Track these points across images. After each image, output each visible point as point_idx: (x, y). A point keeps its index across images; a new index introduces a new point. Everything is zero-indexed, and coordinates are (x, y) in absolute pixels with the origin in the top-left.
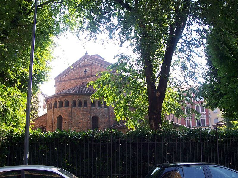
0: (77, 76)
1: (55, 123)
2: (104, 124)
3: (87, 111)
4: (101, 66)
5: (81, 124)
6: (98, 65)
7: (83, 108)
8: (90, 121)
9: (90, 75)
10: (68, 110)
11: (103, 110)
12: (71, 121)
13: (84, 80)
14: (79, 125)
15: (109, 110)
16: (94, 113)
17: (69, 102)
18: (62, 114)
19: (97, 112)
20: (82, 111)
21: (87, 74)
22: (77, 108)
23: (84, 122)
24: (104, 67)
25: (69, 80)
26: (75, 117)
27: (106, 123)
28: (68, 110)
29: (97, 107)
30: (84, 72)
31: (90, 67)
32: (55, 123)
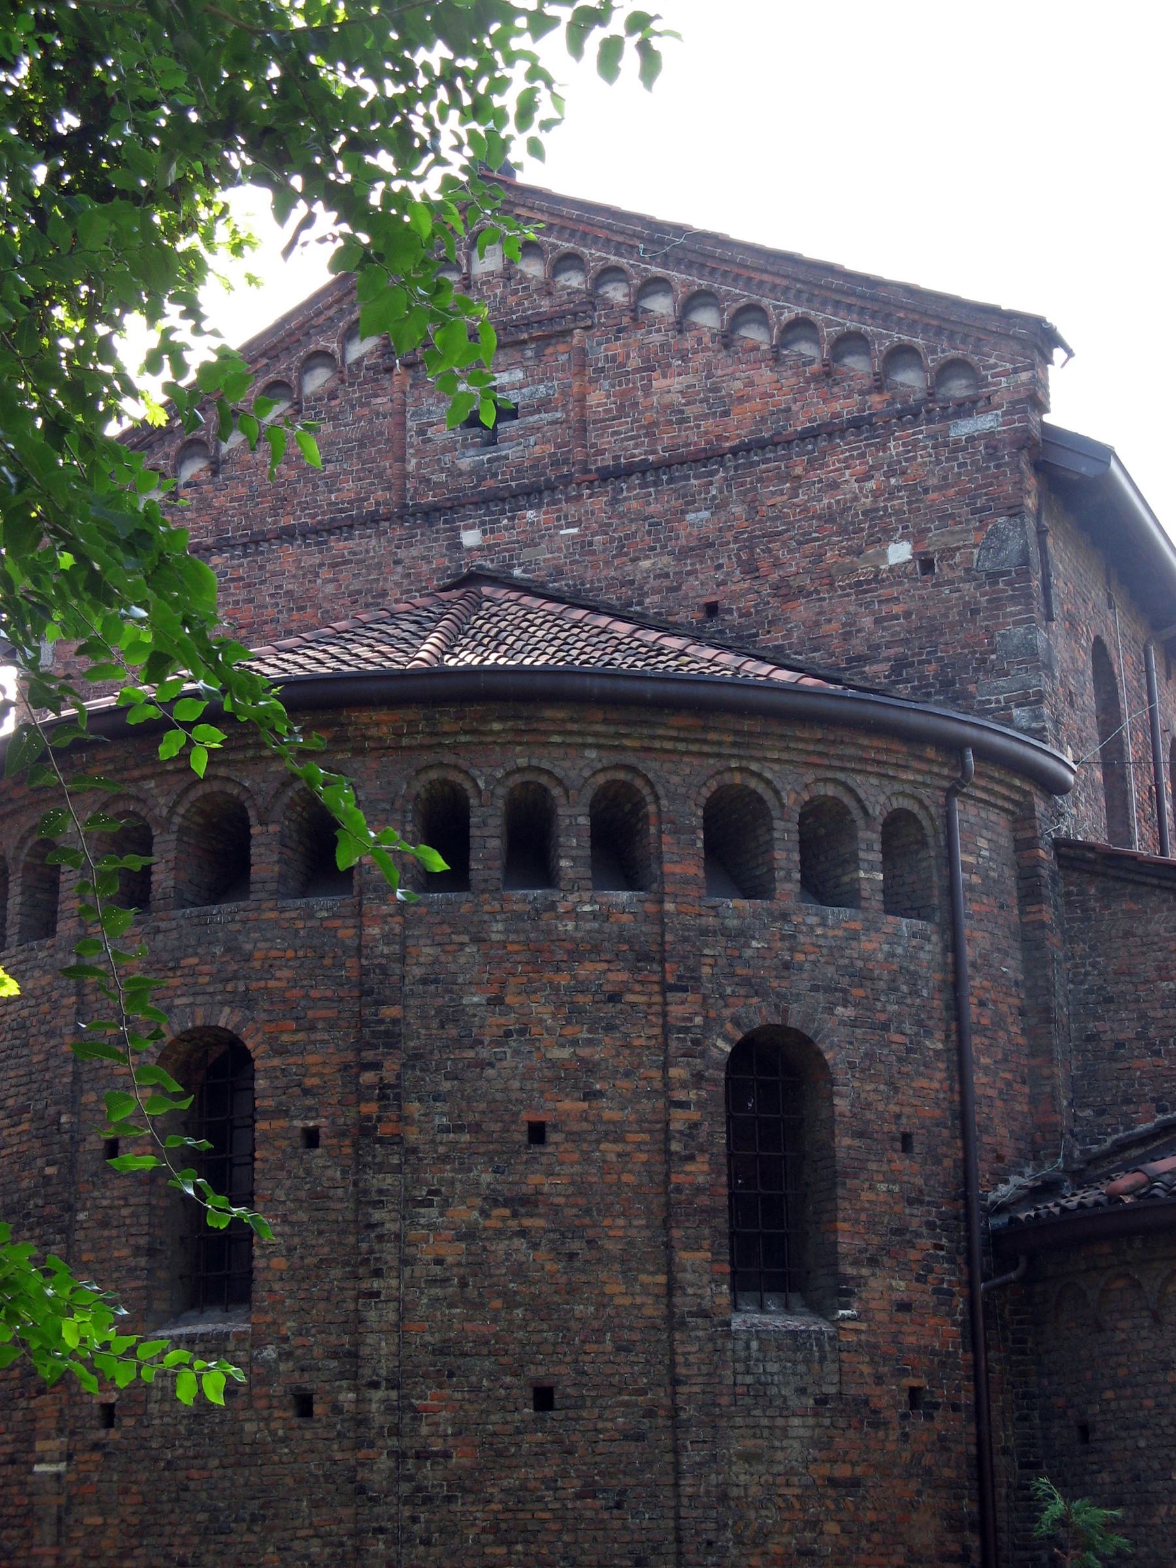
0: (350, 487)
2: (901, 1163)
3: (646, 956)
4: (727, 339)
6: (681, 325)
7: (582, 904)
8: (700, 1111)
10: (347, 934)
11: (872, 944)
13: (471, 538)
14: (535, 1179)
15: (954, 946)
16: (754, 987)
18: (247, 1001)
19: (787, 966)
20: (576, 955)
21: (519, 449)
22: (501, 909)
23: (616, 1133)
24: (783, 344)
25: (222, 545)
26: (458, 1043)
28: (347, 934)
29: (788, 887)
31: (560, 354)
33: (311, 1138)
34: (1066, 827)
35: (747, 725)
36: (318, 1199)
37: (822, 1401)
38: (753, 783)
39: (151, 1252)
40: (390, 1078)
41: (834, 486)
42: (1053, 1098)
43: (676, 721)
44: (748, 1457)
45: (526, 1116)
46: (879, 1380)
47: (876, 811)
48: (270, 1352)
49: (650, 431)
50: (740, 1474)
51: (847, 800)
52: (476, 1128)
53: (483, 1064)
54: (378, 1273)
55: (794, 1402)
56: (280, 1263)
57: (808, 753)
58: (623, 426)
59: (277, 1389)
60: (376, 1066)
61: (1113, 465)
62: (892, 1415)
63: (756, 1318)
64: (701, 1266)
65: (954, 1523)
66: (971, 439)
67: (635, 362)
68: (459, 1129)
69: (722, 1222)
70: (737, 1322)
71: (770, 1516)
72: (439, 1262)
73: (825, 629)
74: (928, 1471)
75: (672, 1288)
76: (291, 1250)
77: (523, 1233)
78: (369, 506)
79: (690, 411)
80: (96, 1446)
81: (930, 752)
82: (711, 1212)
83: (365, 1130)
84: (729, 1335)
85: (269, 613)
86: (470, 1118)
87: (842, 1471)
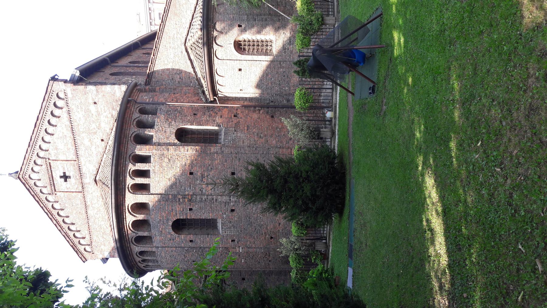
1: (191, 241)
2: (199, 115)
5: (195, 168)
9: (74, 166)
12: (188, 195)
14: (199, 174)
17: (136, 204)
18: (168, 220)
27: (196, 113)
30: (66, 181)
32: (191, 241)
33: (191, 209)
34: (142, 83)
36: (201, 208)
38: (133, 136)
39: (208, 235)
40: (181, 197)
41: (80, 118)
42: (188, 90)
43: (122, 138)
45: (188, 175)
46: (232, 121)
48: (225, 216)
49: (68, 149)
50: (246, 144)
51: (136, 120)
52: (190, 183)
54: (213, 199)
56: (210, 215)
58: (67, 154)
59: (230, 215)
60: (179, 199)
61: (360, 50)
62: (238, 120)
63: (222, 140)
64: (214, 149)
65: (254, 111)
66: (72, 94)
67: (56, 151)
68: (190, 186)
69: (207, 145)
70: (223, 143)
72: (211, 189)
73: (106, 121)
75: (217, 153)
76: (209, 213)
77: (207, 176)
78: (81, 198)
79: (65, 142)
80: (238, 243)
81: (129, 105)
82: (205, 146)
83: (190, 200)
84: (224, 145)
85: (101, 215)
86: (188, 184)
87: (246, 128)
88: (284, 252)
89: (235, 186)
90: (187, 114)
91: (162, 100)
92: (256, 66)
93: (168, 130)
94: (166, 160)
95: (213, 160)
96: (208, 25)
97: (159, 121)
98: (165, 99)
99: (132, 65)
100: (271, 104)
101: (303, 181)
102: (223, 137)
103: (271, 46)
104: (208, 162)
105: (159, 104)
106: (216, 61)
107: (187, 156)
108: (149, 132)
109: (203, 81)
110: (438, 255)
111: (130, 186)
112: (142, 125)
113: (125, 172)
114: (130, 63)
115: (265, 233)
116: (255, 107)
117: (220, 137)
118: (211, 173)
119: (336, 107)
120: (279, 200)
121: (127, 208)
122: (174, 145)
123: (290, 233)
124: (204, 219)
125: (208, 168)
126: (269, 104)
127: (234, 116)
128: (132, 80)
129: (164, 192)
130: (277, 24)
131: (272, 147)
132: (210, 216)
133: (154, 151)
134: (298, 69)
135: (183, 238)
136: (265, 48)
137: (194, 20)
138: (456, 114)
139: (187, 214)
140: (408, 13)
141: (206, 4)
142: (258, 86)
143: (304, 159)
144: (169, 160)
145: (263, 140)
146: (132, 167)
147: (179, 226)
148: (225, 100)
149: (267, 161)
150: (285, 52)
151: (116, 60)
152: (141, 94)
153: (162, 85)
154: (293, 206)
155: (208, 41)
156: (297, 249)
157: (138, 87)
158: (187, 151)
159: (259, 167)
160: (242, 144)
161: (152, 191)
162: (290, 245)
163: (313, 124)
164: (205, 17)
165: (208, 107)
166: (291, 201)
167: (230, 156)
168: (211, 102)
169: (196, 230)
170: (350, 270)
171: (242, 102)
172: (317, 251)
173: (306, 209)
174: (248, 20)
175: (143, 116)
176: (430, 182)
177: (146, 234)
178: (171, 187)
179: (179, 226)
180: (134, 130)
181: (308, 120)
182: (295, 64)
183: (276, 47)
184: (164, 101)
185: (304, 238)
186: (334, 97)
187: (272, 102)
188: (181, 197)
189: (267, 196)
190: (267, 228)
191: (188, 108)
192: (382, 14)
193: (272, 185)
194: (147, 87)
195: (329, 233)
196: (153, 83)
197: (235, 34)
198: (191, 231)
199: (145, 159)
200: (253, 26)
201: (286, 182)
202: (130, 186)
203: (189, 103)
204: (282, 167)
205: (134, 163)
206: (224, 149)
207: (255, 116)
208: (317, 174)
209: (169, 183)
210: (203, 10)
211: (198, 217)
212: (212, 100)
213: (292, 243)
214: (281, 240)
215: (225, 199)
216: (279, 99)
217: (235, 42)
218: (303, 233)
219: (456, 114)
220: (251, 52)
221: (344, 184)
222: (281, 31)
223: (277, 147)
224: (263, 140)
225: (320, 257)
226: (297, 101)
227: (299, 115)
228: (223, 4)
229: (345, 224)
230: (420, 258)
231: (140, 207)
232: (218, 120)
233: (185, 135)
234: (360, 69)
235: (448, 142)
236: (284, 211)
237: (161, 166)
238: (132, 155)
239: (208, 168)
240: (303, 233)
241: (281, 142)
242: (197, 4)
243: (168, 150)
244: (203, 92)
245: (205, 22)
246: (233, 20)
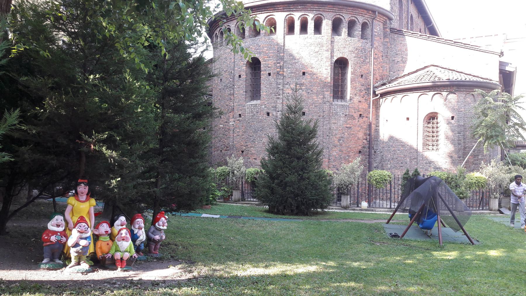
1: (240, 76)
2: (361, 79)
5: (309, 77)
14: (303, 81)
17: (275, 21)
18: (260, 53)
27: (364, 77)
32: (240, 76)
34: (392, 26)
35: (340, 7)
36: (271, 84)
37: (346, 115)
38: (341, 17)
39: (246, 92)
40: (281, 65)
44: (334, 123)
47: (361, 22)
48: (263, 107)
50: (333, 126)
51: (356, 20)
52: (295, 73)
53: (296, 63)
54: (279, 95)
55: (342, 115)
57: (449, 255)
60: (279, 63)
64: (328, 94)
65: (365, 134)
68: (292, 73)
70: (333, 103)
71: (337, 132)
74: (362, 126)
75: (324, 98)
81: (370, 12)
82: (330, 86)
83: (278, 73)
87: (348, 126)
88: (231, 161)
89: (295, 110)
90: (362, 69)
91: (376, 44)
92: (411, 135)
93: (346, 50)
94: (317, 50)
95: (317, 94)
96: (454, 86)
97: (356, 42)
98: (377, 47)
99: (410, 17)
100: (373, 151)
101: (299, 175)
102: (340, 103)
103: (433, 149)
104: (315, 89)
105: (372, 41)
106: (416, 95)
107: (321, 70)
108: (344, 31)
109: (395, 83)
110: (245, 270)
111: (292, 16)
112: (351, 25)
113: (305, 9)
114: (412, 16)
115: (247, 145)
116: (369, 135)
117: (339, 100)
118: (304, 92)
119: (372, 211)
120: (281, 152)
121: (271, 14)
122: (332, 57)
123: (247, 167)
124: (260, 88)
125: (309, 89)
126: (371, 149)
127: (360, 115)
128: (395, 16)
129: (286, 48)
130: (455, 156)
131: (329, 152)
132: (263, 93)
133: (326, 37)
134: (411, 174)
135: (242, 68)
136: (430, 143)
137: (457, 73)
138: (383, 288)
139: (265, 70)
140: (479, 262)
141: (475, 83)
142: (391, 138)
143: (321, 176)
144: (317, 52)
145: (336, 142)
146: (310, 17)
147: (255, 65)
148: (377, 106)
149: (317, 141)
150: (426, 163)
151: (414, 2)
152: (381, 25)
153: (391, 44)
154: (275, 166)
155: (436, 87)
156: (233, 173)
157: (388, 22)
158: (326, 69)
159: (312, 133)
160: (332, 122)
161: (288, 37)
162: (238, 166)
163: (354, 189)
164: (462, 83)
165: (369, 89)
166: (281, 163)
167: (321, 110)
168: (374, 92)
169: (250, 80)
170: (218, 216)
171: (374, 122)
172: (232, 192)
173: (272, 178)
174: (459, 126)
175: (360, 26)
176: (312, 268)
177: (247, 33)
178: (291, 55)
179: (255, 65)
180: (346, 18)
181: (358, 184)
182: (416, 171)
183: (431, 155)
184: (375, 46)
185: (244, 180)
186: (382, 209)
187: (375, 152)
188: (281, 65)
189: (285, 140)
190: (251, 147)
191: (368, 70)
192: (473, 244)
193: (294, 146)
194: (388, 30)
195: (248, 204)
196: (393, 35)
197: (444, 114)
198: (250, 76)
199: (318, 28)
200: (453, 131)
201: (299, 158)
202: (292, 16)
203: (374, 70)
204: (312, 156)
205: (314, 18)
206: (328, 104)
207: (361, 135)
208: (306, 188)
209: (294, 53)
210: (468, 82)
211: (262, 82)
212: (377, 93)
213: (239, 168)
214: (241, 158)
215: (280, 107)
216: (378, 159)
217: (437, 113)
218: (248, 178)
219: (383, 288)
220: (426, 129)
221: (297, 214)
222: (449, 160)
223: (329, 156)
224: (336, 142)
225: (227, 194)
226: (376, 173)
227: (363, 175)
228: (475, 101)
229: (259, 214)
230: (239, 258)
231: (272, 24)
232: (356, 99)
233: (341, 68)
234: (415, 224)
235: (355, 281)
236: (269, 157)
237: (311, 45)
238: (322, 17)
239: (309, 89)
240: (248, 178)
241: (335, 161)
242: (474, 76)
243: (327, 51)
244: (384, 84)
245: (456, 83)
246: (459, 111)
